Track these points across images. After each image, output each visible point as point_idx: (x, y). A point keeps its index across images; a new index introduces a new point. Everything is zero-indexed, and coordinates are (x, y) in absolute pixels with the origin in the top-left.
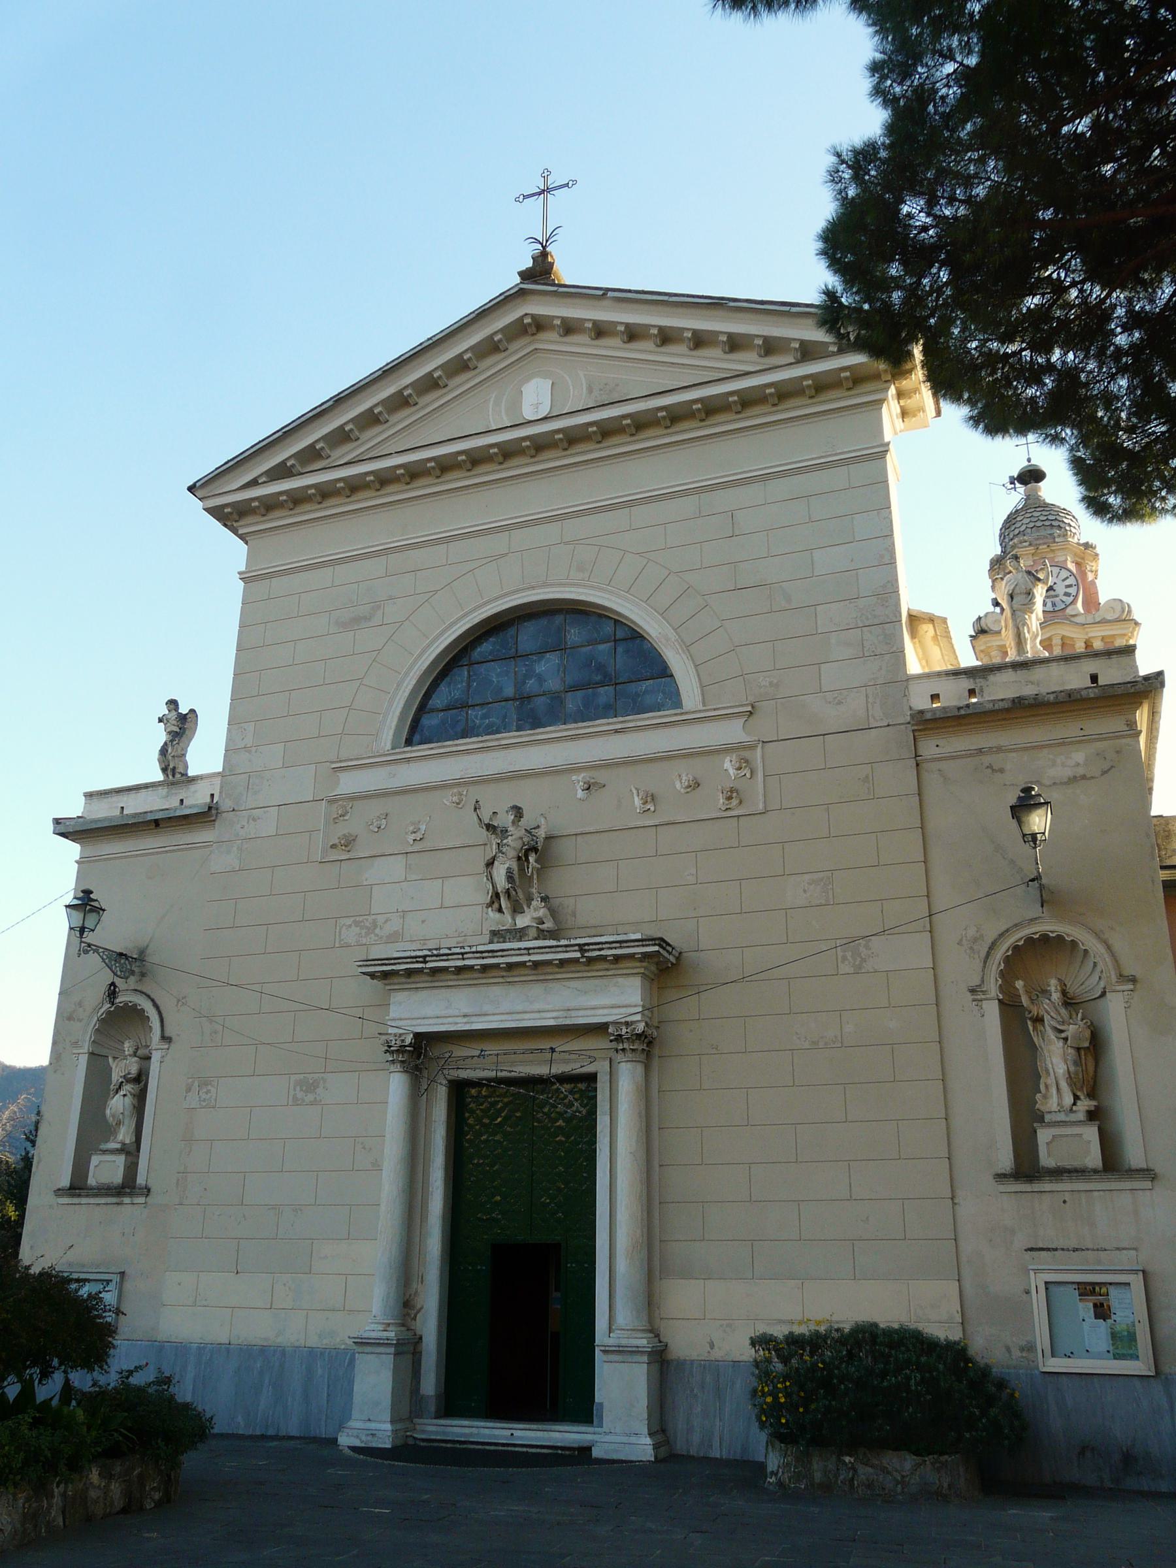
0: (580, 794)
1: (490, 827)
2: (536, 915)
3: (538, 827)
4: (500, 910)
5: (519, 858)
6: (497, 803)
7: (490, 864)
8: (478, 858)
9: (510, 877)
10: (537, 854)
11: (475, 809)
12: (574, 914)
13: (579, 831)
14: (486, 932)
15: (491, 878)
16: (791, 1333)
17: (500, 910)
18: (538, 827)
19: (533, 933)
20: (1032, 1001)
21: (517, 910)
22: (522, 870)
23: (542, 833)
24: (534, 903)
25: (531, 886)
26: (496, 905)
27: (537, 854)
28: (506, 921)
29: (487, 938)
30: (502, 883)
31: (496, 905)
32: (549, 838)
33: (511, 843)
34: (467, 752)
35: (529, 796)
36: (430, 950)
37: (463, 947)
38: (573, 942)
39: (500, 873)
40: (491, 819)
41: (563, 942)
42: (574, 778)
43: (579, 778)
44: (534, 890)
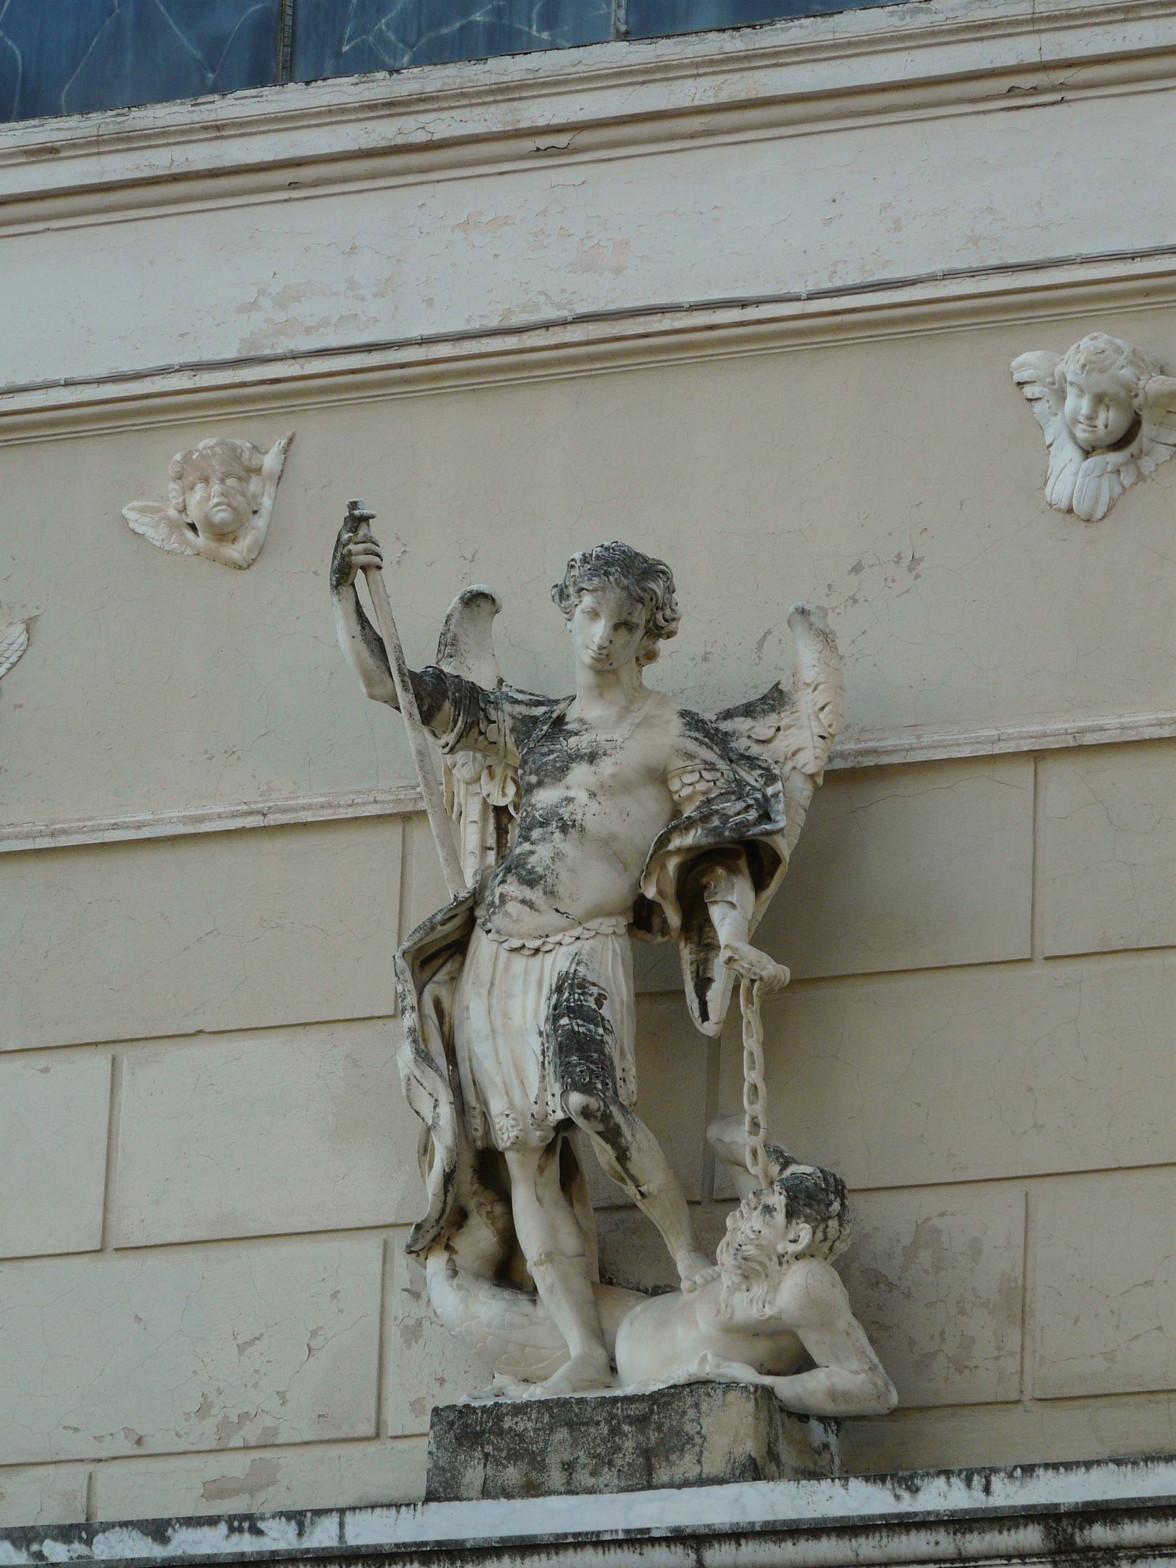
0: (1068, 475)
1: (445, 701)
2: (749, 1306)
3: (774, 700)
4: (507, 1271)
5: (642, 916)
6: (490, 531)
7: (441, 951)
8: (371, 904)
9: (577, 1045)
10: (758, 883)
11: (343, 574)
12: (1017, 1306)
13: (1057, 727)
14: (408, 1417)
15: (444, 1048)
16: (462, 598)
17: (507, 1271)
18: (774, 700)
19: (730, 1429)
20: (907, 1469)
21: (622, 1269)
22: (657, 995)
23: (799, 744)
24: (744, 1225)
25: (717, 1105)
26: (478, 1238)
27: (758, 883)
28: (547, 1344)
29: (412, 1463)
30: (520, 1084)
31: (478, 1238)
32: (849, 779)
33: (584, 807)
34: (293, 176)
35: (701, 482)
36: (298, 1518)
37: (247, 1523)
38: (1007, 1494)
39: (507, 1014)
40: (449, 644)
41: (940, 1496)
42: (1029, 362)
43: (1066, 365)
44: (740, 1138)
